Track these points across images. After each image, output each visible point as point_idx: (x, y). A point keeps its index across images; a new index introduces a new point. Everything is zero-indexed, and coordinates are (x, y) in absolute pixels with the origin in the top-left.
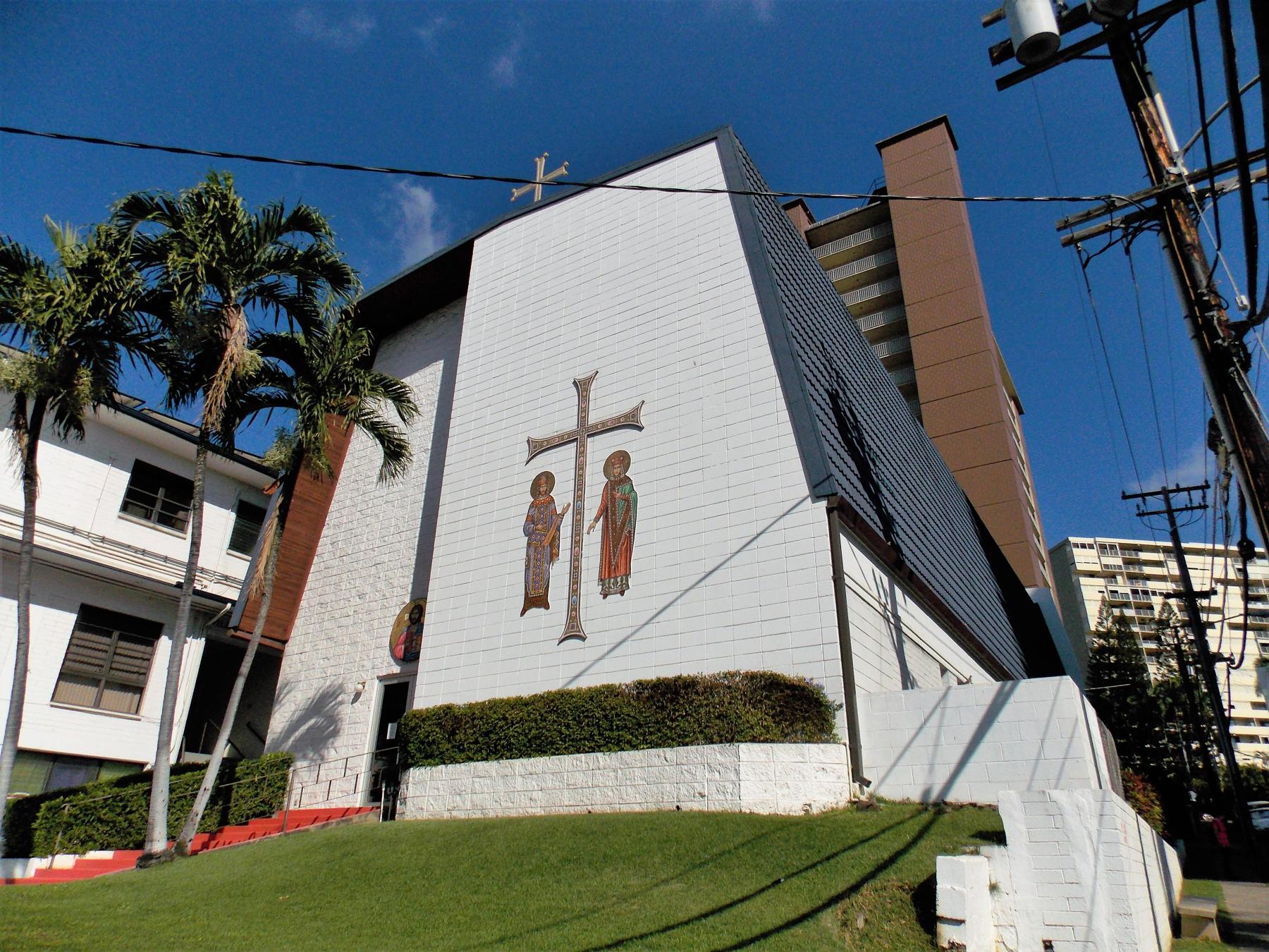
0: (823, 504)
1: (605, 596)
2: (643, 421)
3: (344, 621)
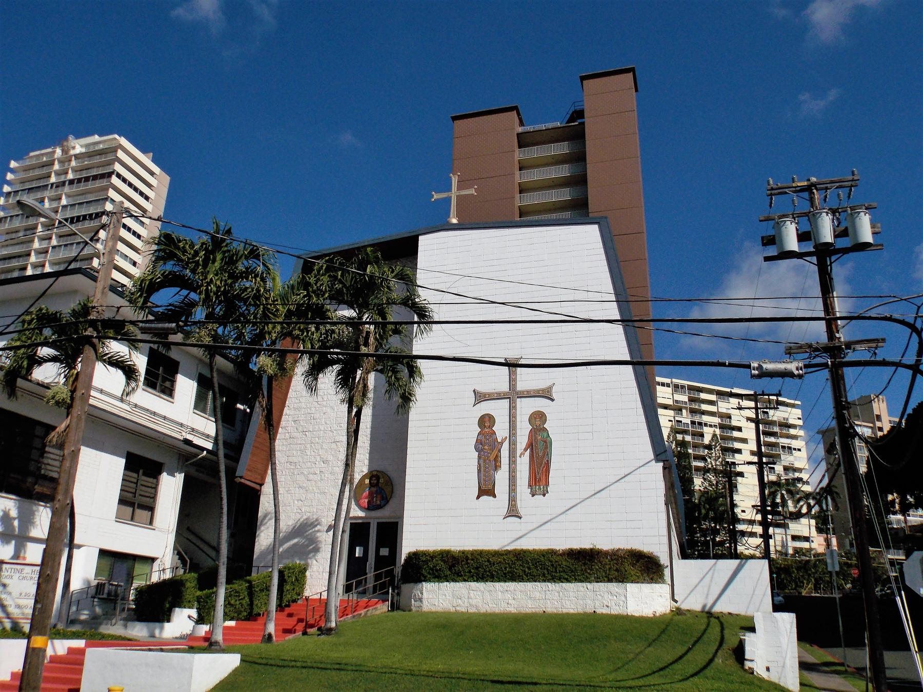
0: (661, 464)
1: (533, 495)
2: (554, 396)
3: (311, 477)
